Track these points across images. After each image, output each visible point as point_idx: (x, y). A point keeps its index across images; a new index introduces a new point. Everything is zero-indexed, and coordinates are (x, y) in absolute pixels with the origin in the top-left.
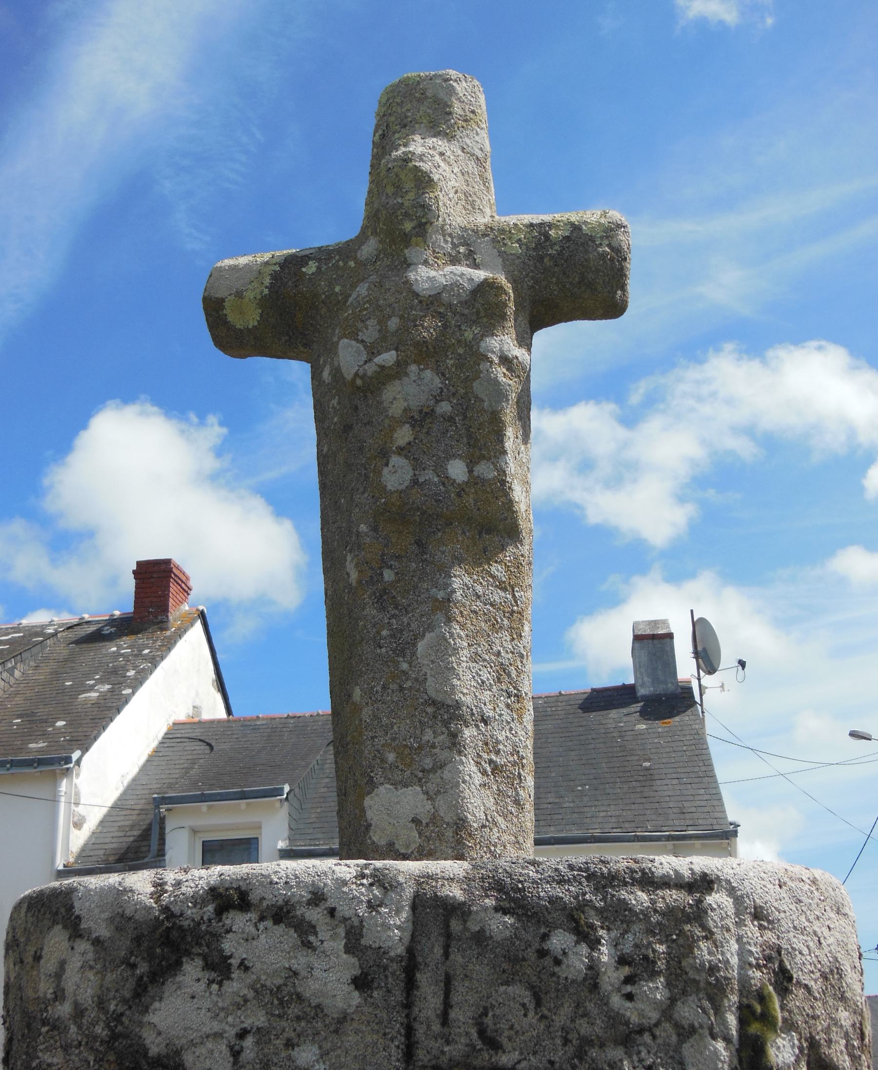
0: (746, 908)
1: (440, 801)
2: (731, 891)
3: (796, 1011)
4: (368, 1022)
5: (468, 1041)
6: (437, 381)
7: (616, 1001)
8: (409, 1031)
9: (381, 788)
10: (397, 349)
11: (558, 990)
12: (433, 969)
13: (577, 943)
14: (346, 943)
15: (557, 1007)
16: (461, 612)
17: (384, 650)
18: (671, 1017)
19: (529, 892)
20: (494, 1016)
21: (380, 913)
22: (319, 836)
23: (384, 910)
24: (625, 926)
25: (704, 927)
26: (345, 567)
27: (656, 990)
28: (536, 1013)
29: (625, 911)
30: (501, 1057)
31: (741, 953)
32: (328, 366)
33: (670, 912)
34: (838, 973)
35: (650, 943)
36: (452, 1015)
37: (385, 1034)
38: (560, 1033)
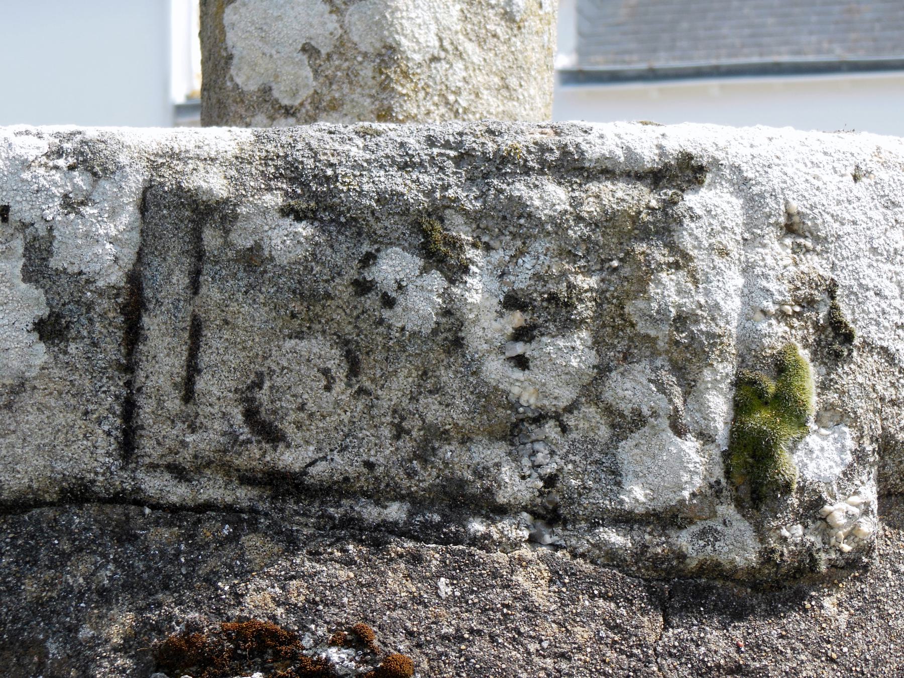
0: (769, 216)
1: (353, 15)
2: (741, 183)
3: (855, 391)
4: (60, 393)
5: (226, 428)
8: (129, 408)
11: (389, 349)
12: (168, 311)
13: (425, 270)
14: (25, 265)
15: (386, 377)
18: (598, 397)
19: (343, 183)
20: (271, 388)
21: (83, 216)
22: (633, 46)
23: (88, 210)
24: (519, 243)
25: (673, 248)
27: (571, 352)
28: (349, 385)
29: (519, 218)
30: (282, 454)
31: (747, 295)
33: (609, 221)
35: (564, 274)
36: (201, 384)
37: (86, 413)
38: (389, 419)
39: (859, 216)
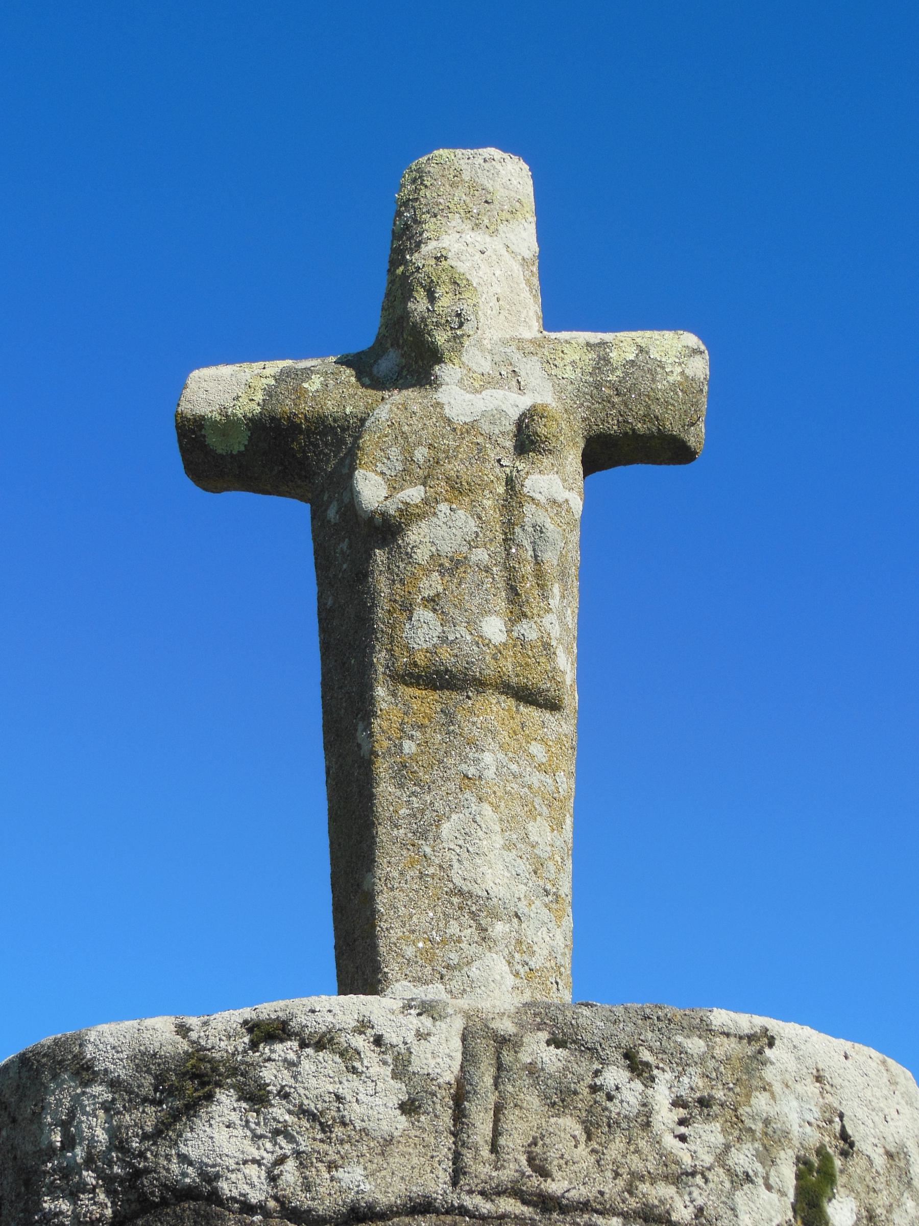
5: (517, 1167)
6: (472, 525)
7: (670, 1142)
9: (397, 985)
10: (424, 484)
16: (495, 793)
17: (402, 831)
26: (355, 738)
32: (335, 503)
34: (905, 1158)
36: (502, 1141)
39: (851, 1079)
